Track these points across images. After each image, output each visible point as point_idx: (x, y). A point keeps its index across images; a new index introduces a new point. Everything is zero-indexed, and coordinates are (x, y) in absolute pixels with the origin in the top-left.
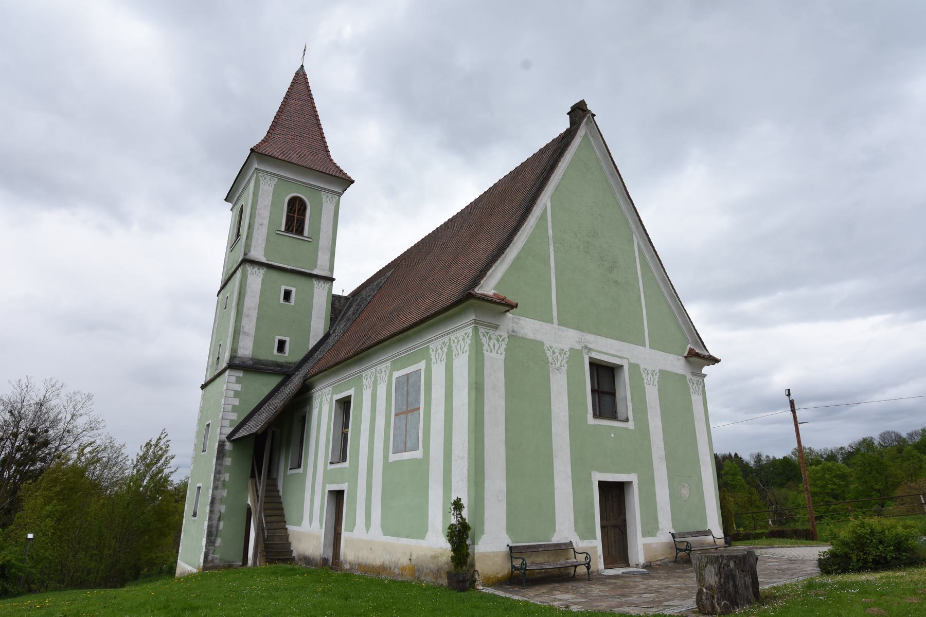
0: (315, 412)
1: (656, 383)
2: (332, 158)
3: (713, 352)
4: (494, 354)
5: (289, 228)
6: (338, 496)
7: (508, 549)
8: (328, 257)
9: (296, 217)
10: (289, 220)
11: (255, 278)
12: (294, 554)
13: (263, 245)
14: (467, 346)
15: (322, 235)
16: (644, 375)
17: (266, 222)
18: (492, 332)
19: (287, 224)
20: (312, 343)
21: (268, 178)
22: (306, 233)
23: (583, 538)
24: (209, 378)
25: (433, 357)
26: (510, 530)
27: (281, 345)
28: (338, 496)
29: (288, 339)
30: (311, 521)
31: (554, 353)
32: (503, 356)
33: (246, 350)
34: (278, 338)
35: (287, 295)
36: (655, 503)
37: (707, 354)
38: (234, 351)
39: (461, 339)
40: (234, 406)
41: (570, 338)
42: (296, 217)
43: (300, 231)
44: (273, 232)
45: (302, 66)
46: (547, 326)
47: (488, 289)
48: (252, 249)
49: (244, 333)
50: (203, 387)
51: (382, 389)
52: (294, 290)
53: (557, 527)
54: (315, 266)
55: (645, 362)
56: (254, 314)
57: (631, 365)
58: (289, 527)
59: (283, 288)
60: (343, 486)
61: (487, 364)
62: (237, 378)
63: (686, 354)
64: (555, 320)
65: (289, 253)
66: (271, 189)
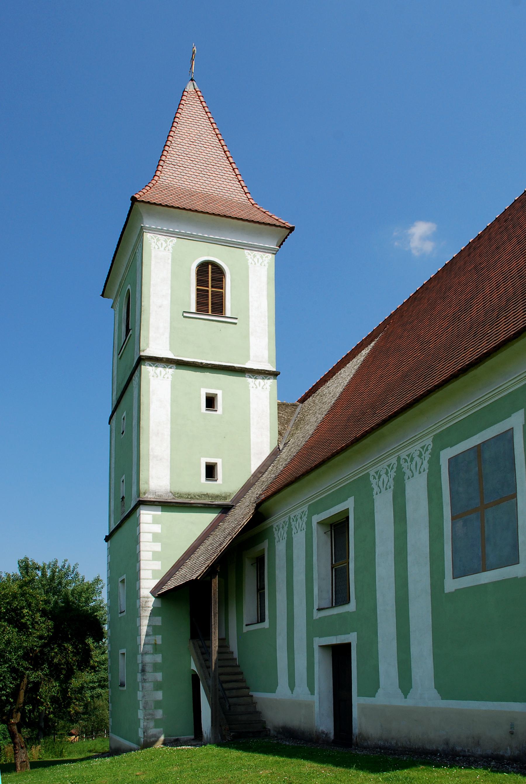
0: (281, 547)
5: (202, 306)
6: (340, 655)
10: (201, 295)
12: (269, 726)
13: (167, 335)
14: (426, 463)
17: (167, 302)
19: (198, 303)
20: (255, 464)
22: (228, 313)
24: (113, 527)
25: (374, 486)
27: (211, 471)
28: (340, 655)
29: (219, 461)
30: (292, 686)
35: (211, 402)
39: (383, 472)
40: (154, 553)
50: (107, 539)
51: (417, 489)
54: (248, 358)
58: (258, 695)
60: (352, 638)
62: (154, 516)
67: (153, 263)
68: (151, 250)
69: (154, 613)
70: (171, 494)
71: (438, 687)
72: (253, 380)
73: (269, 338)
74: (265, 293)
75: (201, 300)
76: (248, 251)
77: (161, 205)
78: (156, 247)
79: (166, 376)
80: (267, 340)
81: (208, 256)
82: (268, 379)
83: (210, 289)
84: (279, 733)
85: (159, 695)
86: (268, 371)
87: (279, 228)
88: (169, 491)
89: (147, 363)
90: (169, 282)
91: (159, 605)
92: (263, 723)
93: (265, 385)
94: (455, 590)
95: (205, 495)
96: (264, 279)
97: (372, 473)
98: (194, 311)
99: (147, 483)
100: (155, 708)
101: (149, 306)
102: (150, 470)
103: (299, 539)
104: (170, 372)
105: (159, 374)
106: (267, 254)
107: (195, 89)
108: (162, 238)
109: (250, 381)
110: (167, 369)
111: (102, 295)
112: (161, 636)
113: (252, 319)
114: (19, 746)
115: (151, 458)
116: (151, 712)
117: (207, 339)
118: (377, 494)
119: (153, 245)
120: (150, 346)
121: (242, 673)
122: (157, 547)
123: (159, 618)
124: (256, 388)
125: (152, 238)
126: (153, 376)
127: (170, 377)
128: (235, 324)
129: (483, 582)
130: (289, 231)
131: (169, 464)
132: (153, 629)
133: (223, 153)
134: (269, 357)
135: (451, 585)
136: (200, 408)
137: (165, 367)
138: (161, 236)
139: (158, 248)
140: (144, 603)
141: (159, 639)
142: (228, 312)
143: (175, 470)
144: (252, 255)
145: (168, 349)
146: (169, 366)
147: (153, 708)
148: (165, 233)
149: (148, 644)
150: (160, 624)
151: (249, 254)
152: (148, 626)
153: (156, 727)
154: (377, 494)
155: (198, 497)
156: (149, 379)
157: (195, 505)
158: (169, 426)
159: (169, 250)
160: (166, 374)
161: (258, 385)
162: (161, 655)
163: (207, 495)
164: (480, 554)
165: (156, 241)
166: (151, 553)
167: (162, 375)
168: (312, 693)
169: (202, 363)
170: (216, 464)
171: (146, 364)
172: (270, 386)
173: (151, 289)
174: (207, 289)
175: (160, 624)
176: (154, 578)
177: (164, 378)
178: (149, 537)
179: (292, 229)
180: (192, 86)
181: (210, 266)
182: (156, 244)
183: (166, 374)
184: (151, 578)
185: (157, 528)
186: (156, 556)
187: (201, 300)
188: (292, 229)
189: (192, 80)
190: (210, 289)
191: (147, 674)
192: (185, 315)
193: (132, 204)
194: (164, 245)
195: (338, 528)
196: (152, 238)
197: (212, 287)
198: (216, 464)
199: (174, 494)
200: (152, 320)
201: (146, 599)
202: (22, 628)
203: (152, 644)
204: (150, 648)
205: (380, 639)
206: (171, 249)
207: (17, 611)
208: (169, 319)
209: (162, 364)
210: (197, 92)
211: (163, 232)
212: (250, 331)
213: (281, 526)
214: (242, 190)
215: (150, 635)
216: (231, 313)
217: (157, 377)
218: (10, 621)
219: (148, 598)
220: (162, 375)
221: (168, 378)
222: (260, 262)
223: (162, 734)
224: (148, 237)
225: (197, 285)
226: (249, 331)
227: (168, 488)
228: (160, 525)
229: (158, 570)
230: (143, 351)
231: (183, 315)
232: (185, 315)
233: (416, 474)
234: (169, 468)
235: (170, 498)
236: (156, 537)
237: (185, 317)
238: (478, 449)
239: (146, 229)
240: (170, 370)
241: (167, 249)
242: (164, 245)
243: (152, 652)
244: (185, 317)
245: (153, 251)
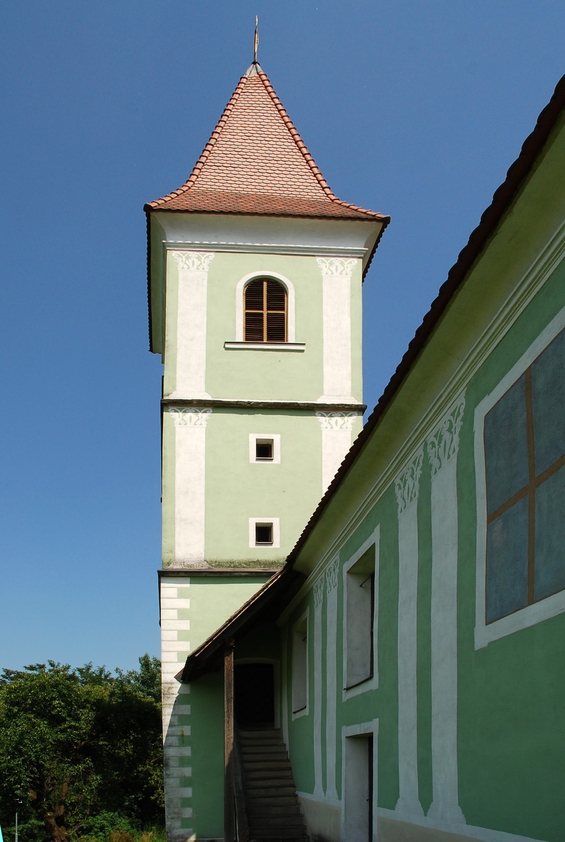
12: (309, 834)
14: (456, 438)
17: (201, 334)
27: (264, 534)
35: (264, 450)
40: (180, 632)
43: (278, 333)
58: (303, 795)
60: (373, 726)
62: (179, 589)
64: (261, 312)
67: (181, 286)
68: (178, 271)
69: (180, 701)
70: (205, 563)
71: (463, 803)
72: (327, 418)
73: (353, 366)
74: (347, 308)
75: (253, 327)
76: (322, 258)
77: (187, 211)
79: (199, 422)
81: (262, 270)
82: (349, 416)
83: (266, 312)
85: (188, 792)
86: (349, 405)
87: (366, 222)
88: (203, 559)
89: (171, 408)
90: (205, 309)
91: (187, 691)
92: (305, 828)
93: (344, 423)
94: (489, 643)
95: (254, 562)
96: (346, 292)
97: (398, 481)
98: (242, 341)
99: (172, 551)
100: (182, 806)
101: (176, 340)
102: (177, 536)
104: (204, 418)
106: (351, 259)
107: (258, 74)
108: (193, 255)
109: (323, 420)
110: (200, 414)
111: (151, 350)
112: (189, 727)
114: (58, 840)
115: (177, 521)
116: (176, 810)
117: (263, 373)
118: (401, 511)
119: (181, 264)
120: (177, 388)
121: (290, 769)
122: (185, 625)
123: (188, 707)
125: (179, 256)
126: (180, 424)
127: (205, 424)
128: (302, 351)
129: (528, 624)
130: (380, 225)
131: (203, 527)
132: (179, 719)
133: (294, 144)
134: (352, 389)
135: (484, 635)
137: (196, 412)
138: (192, 253)
139: (189, 268)
140: (166, 690)
141: (187, 730)
142: (291, 336)
143: (210, 534)
144: (327, 263)
145: (204, 390)
146: (203, 411)
147: (179, 806)
148: (198, 247)
149: (172, 736)
150: (189, 713)
151: (323, 262)
152: (172, 715)
153: (183, 826)
154: (401, 511)
155: (245, 565)
156: (174, 429)
157: (237, 574)
158: (203, 483)
159: (203, 269)
160: (198, 419)
161: (334, 425)
162: (190, 748)
163: (258, 563)
164: (526, 573)
165: (184, 259)
166: (176, 632)
167: (193, 422)
168: (340, 798)
169: (249, 403)
170: (272, 524)
171: (169, 410)
172: (352, 424)
173: (179, 320)
174: (261, 312)
175: (189, 713)
176: (180, 661)
177: (195, 424)
178: (174, 614)
179: (386, 221)
180: (254, 71)
181: (265, 284)
182: (186, 263)
183: (198, 419)
184: (176, 660)
185: (185, 604)
186: (182, 636)
187: (253, 327)
188: (386, 221)
189: (254, 63)
190: (266, 312)
191: (171, 769)
192: (227, 346)
193: (148, 216)
195: (364, 572)
196: (179, 256)
197: (268, 309)
198: (272, 524)
199: (210, 563)
200: (180, 358)
201: (170, 685)
202: (55, 721)
203: (177, 736)
204: (175, 740)
205: (400, 728)
207: (48, 703)
208: (204, 354)
209: (193, 408)
210: (260, 75)
211: (194, 247)
212: (324, 358)
213: (319, 586)
214: (319, 185)
215: (175, 726)
216: (296, 338)
217: (186, 424)
218: (38, 715)
219: (172, 683)
220: (193, 422)
221: (201, 424)
222: (339, 271)
223: (191, 835)
224: (173, 256)
225: (247, 309)
226: (322, 359)
227: (202, 557)
228: (189, 600)
230: (168, 395)
231: (224, 347)
232: (227, 346)
233: (444, 460)
234: (204, 532)
235: (205, 567)
236: (182, 614)
237: (227, 349)
238: (528, 378)
239: (169, 246)
240: (205, 414)
242: (197, 262)
243: (177, 744)
244: (227, 349)
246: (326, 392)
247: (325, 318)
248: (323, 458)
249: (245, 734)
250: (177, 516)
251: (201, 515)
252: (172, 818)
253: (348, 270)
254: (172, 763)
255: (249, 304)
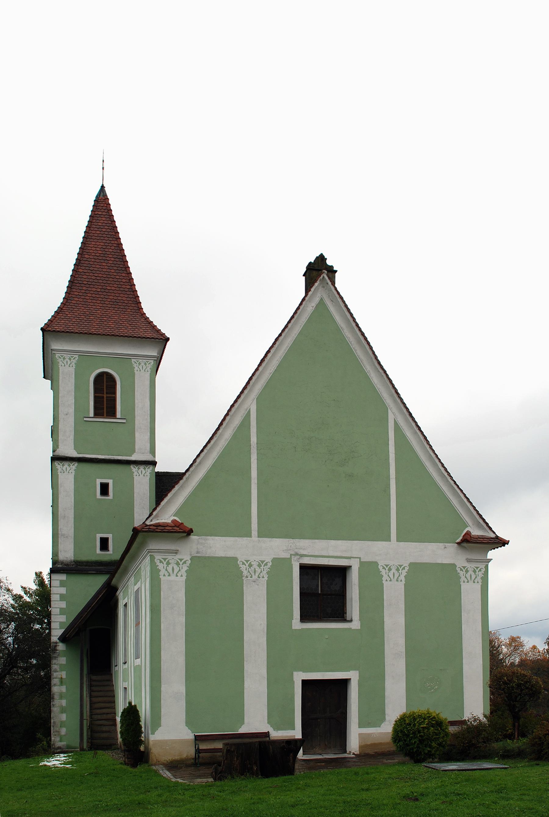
1: (402, 577)
2: (145, 311)
3: (501, 534)
4: (173, 577)
5: (98, 413)
7: (194, 738)
8: (147, 436)
9: (105, 396)
11: (68, 473)
13: (72, 437)
15: (138, 412)
16: (383, 572)
17: (72, 410)
18: (170, 557)
21: (67, 356)
22: (118, 415)
23: (277, 728)
26: (189, 723)
27: (104, 544)
29: (110, 536)
31: (250, 565)
32: (184, 578)
33: (68, 554)
34: (99, 536)
36: (383, 697)
37: (493, 536)
38: (55, 554)
40: (61, 609)
41: (277, 547)
42: (105, 396)
43: (112, 413)
44: (80, 421)
45: (103, 187)
46: (242, 541)
47: (167, 516)
48: (60, 444)
49: (63, 535)
52: (110, 482)
53: (246, 720)
55: (384, 561)
56: (71, 514)
57: (363, 564)
59: (99, 482)
61: (164, 587)
63: (459, 540)
64: (255, 533)
65: (104, 439)
66: (72, 370)
67: (61, 378)
78: (63, 365)
80: (149, 435)
84: (492, 758)
93: (180, 570)
103: (122, 609)
104: (74, 466)
105: (65, 471)
111: (44, 377)
113: (137, 418)
115: (60, 536)
116: (57, 729)
122: (63, 605)
124: (169, 575)
130: (165, 342)
136: (95, 495)
161: (140, 473)
174: (255, 533)
192: (85, 419)
194: (69, 362)
206: (74, 365)
219: (56, 643)
222: (144, 369)
229: (64, 622)
232: (85, 419)
241: (71, 366)
242: (69, 362)
245: (60, 368)
246: (136, 451)
247: (136, 401)
248: (135, 495)
249: (94, 677)
250: (60, 533)
251: (71, 532)
252: (55, 735)
253: (148, 369)
254: (56, 697)
255: (97, 390)
